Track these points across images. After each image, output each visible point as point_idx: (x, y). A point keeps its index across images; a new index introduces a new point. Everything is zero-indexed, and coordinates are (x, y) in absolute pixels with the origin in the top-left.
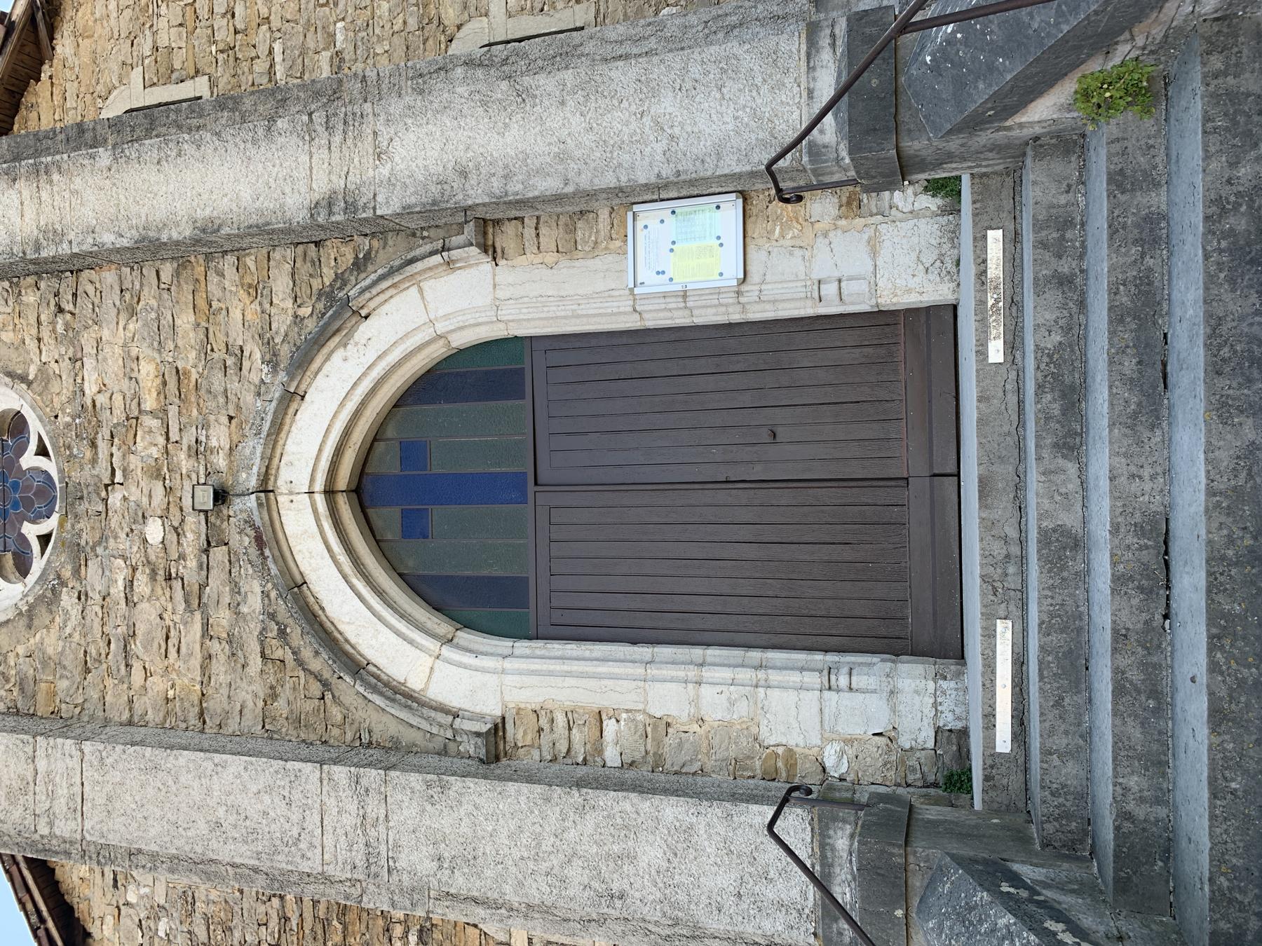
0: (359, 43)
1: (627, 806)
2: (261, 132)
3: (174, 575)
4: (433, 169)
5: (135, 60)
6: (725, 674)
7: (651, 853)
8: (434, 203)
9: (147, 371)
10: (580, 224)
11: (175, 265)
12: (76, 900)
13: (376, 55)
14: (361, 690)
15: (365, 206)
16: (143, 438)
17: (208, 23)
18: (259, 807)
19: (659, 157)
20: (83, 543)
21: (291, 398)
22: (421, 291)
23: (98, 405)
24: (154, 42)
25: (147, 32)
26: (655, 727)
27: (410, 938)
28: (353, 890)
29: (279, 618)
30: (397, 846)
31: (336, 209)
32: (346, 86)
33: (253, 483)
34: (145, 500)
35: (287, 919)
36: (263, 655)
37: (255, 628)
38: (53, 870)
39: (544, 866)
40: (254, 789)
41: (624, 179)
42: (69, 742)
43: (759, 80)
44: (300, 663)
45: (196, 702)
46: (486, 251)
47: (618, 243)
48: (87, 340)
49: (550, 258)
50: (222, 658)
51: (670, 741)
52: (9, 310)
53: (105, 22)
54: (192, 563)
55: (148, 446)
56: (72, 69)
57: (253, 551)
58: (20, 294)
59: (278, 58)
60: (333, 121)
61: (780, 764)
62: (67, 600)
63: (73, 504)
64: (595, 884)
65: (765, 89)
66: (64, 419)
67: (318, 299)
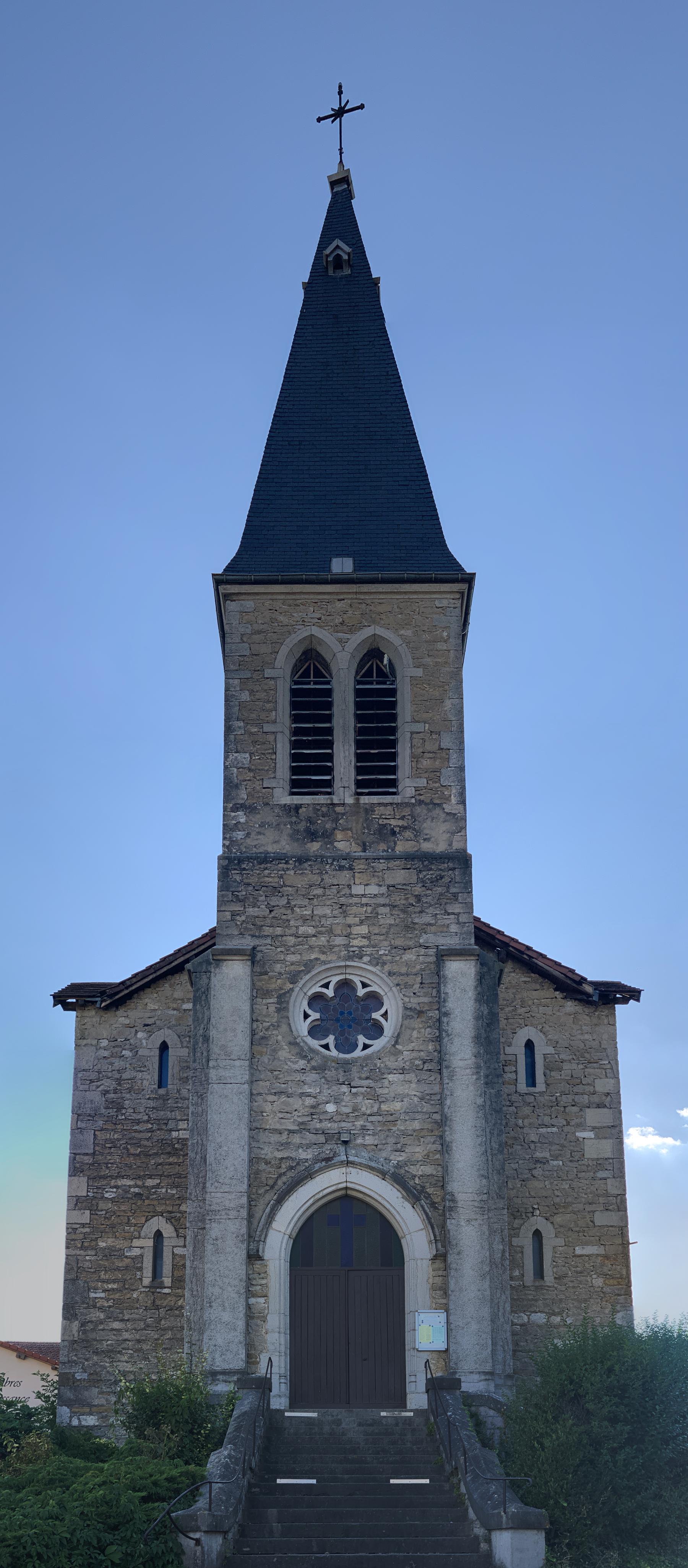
0: (551, 1173)
1: (241, 1309)
2: (482, 1172)
3: (314, 1116)
4: (461, 1242)
5: (559, 1049)
6: (283, 1342)
7: (226, 1316)
8: (450, 1242)
9: (397, 1106)
10: (442, 1292)
11: (439, 1121)
12: (135, 1000)
13: (545, 1181)
14: (272, 1203)
15: (451, 1215)
16: (369, 1103)
17: (571, 1092)
18: (229, 1165)
19: (457, 1324)
20: (326, 1072)
21: (383, 1174)
22: (422, 1230)
23: (384, 1081)
24: (565, 1061)
25: (571, 1057)
26: (263, 1317)
27: (137, 1189)
28: (193, 1196)
29: (298, 1167)
30: (220, 1223)
31: (451, 1203)
32: (502, 1200)
33: (351, 1158)
34: (344, 1104)
35: (138, 1124)
36: (282, 1159)
37: (293, 1154)
38: (150, 987)
39: (218, 1279)
40: (236, 1164)
41: (451, 1311)
42: (248, 1077)
43: (478, 1356)
44: (280, 1176)
45: (262, 1127)
46: (434, 1256)
47: (434, 1306)
48: (412, 1076)
49: (431, 1281)
50: (280, 1139)
51: (259, 1322)
52: (426, 1035)
53: (580, 1032)
54: (318, 1126)
55: (367, 1106)
56: (559, 1011)
57: (323, 1156)
58: (433, 1041)
59: (549, 1130)
60: (482, 1203)
61: (253, 1360)
62: (302, 1063)
63: (342, 1067)
64: (214, 1297)
65: (475, 1358)
66: (378, 1062)
67: (421, 1186)
